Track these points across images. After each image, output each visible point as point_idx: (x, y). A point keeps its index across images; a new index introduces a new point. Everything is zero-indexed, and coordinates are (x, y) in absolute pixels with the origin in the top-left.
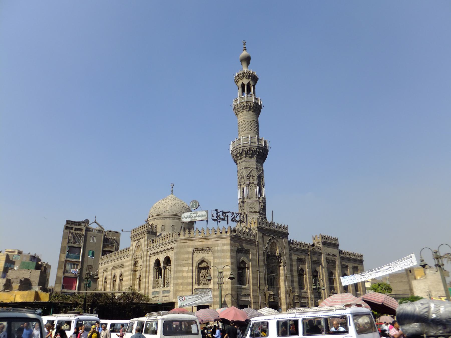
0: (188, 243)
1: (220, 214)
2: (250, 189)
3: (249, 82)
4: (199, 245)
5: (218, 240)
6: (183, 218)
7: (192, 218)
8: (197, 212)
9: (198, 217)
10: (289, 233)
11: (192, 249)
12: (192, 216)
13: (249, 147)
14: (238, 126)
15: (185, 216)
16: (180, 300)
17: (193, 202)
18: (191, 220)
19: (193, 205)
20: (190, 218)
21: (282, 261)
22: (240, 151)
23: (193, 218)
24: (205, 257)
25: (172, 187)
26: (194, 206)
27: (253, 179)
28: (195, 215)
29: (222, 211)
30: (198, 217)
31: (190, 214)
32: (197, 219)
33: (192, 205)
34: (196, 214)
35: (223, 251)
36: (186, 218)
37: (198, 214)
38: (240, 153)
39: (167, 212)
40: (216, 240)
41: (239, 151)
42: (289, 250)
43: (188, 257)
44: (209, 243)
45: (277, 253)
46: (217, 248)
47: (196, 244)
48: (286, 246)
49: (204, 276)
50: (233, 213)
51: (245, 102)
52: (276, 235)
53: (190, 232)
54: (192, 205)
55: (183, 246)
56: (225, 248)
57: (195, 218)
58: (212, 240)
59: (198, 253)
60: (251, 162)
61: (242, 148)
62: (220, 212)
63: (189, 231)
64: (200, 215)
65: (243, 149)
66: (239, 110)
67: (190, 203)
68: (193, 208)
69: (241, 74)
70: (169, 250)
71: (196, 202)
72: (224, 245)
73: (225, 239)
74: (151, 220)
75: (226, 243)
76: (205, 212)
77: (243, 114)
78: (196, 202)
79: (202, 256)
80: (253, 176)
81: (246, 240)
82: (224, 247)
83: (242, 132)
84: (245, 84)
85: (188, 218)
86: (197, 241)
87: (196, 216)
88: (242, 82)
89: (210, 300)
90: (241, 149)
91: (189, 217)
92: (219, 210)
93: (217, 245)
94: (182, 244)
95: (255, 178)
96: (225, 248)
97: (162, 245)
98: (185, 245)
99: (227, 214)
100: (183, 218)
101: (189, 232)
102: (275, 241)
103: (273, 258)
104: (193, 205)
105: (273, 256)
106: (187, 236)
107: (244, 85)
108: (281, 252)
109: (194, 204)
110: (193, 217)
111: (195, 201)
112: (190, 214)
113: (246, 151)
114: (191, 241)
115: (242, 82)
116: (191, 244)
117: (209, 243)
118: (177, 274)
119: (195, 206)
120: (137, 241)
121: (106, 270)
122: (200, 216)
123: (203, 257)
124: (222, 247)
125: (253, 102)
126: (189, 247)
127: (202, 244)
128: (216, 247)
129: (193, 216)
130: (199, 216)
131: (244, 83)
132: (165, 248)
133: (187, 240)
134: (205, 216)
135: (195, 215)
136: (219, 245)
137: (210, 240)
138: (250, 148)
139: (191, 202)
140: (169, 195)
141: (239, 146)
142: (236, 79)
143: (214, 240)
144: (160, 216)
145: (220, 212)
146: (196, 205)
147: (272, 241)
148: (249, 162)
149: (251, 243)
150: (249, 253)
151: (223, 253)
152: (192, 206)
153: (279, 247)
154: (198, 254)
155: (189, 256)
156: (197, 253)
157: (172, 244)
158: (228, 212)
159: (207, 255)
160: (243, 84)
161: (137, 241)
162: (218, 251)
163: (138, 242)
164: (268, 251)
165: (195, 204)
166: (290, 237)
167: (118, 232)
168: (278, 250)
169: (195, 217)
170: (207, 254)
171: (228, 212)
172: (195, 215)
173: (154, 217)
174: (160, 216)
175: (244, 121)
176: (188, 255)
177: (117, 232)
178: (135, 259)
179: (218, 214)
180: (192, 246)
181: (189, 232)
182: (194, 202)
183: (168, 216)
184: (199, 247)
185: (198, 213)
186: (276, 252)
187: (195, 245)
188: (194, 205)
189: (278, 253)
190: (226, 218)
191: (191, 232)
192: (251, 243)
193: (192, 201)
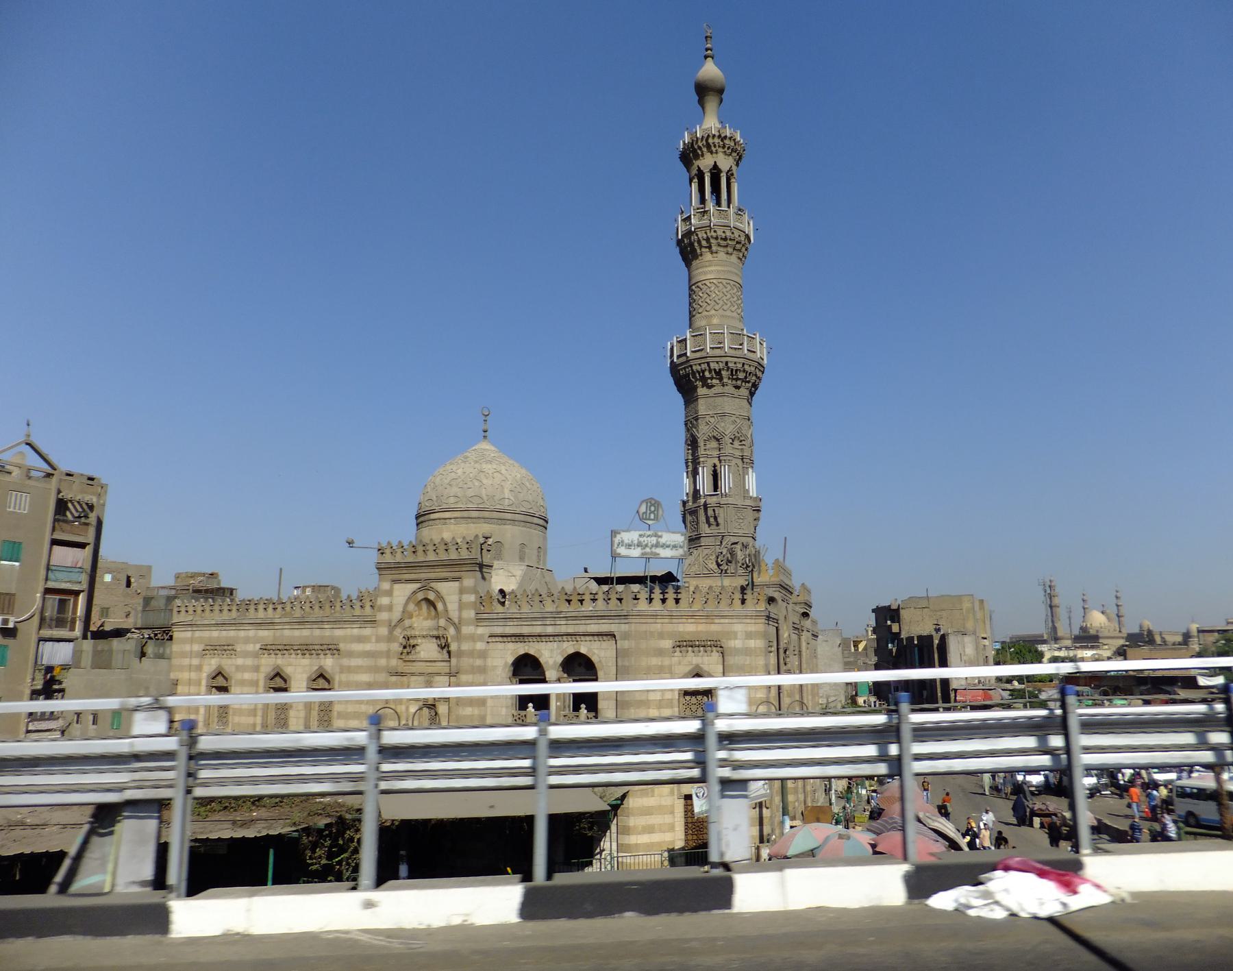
0: (659, 625)
4: (688, 633)
5: (735, 621)
6: (618, 545)
7: (644, 549)
8: (660, 534)
9: (661, 549)
11: (671, 641)
12: (646, 542)
14: (742, 297)
15: (626, 541)
16: (697, 796)
17: (649, 504)
18: (642, 554)
19: (648, 512)
20: (639, 548)
23: (648, 550)
24: (701, 666)
25: (484, 418)
26: (650, 516)
28: (654, 540)
30: (662, 546)
31: (640, 536)
32: (659, 554)
33: (645, 511)
34: (657, 540)
35: (747, 652)
36: (629, 546)
37: (662, 541)
39: (507, 502)
40: (730, 621)
43: (660, 664)
44: (714, 628)
46: (733, 642)
47: (681, 628)
51: (730, 227)
53: (664, 596)
54: (646, 513)
55: (646, 632)
56: (752, 643)
57: (654, 550)
58: (722, 621)
59: (684, 654)
60: (738, 400)
61: (724, 359)
63: (661, 591)
64: (668, 543)
65: (727, 363)
67: (640, 507)
68: (646, 519)
69: (714, 136)
70: (588, 638)
71: (656, 505)
72: (749, 636)
73: (753, 621)
74: (452, 521)
75: (755, 632)
76: (682, 535)
77: (716, 259)
78: (656, 505)
79: (694, 662)
80: (741, 439)
82: (751, 641)
84: (723, 170)
85: (633, 547)
86: (684, 620)
87: (657, 545)
88: (715, 162)
89: (764, 792)
90: (722, 362)
91: (638, 546)
93: (734, 635)
94: (644, 628)
95: (744, 445)
96: (752, 643)
97: (555, 618)
98: (652, 630)
100: (618, 545)
101: (661, 593)
104: (648, 512)
106: (657, 604)
107: (720, 171)
109: (650, 510)
110: (646, 545)
111: (653, 502)
112: (640, 536)
114: (666, 621)
115: (715, 162)
116: (669, 628)
117: (714, 628)
118: (633, 711)
119: (654, 514)
120: (418, 585)
122: (668, 546)
123: (697, 666)
124: (747, 641)
125: (744, 232)
126: (661, 636)
127: (695, 630)
128: (731, 639)
129: (647, 543)
130: (664, 546)
132: (563, 629)
133: (659, 617)
134: (681, 547)
135: (655, 542)
136: (739, 634)
137: (717, 621)
138: (743, 364)
139: (643, 502)
140: (473, 446)
141: (717, 352)
143: (727, 621)
144: (486, 514)
146: (656, 512)
148: (734, 399)
151: (748, 658)
152: (643, 513)
154: (684, 655)
155: (662, 661)
156: (679, 654)
157: (604, 621)
159: (706, 659)
160: (715, 166)
161: (418, 585)
162: (737, 651)
165: (653, 509)
167: (94, 477)
169: (652, 546)
170: (707, 658)
172: (654, 540)
173: (465, 514)
174: (486, 514)
175: (720, 281)
176: (660, 659)
177: (91, 479)
180: (670, 635)
181: (661, 593)
182: (650, 502)
183: (509, 516)
184: (688, 638)
185: (661, 537)
187: (679, 632)
188: (653, 512)
191: (666, 596)
193: (646, 501)
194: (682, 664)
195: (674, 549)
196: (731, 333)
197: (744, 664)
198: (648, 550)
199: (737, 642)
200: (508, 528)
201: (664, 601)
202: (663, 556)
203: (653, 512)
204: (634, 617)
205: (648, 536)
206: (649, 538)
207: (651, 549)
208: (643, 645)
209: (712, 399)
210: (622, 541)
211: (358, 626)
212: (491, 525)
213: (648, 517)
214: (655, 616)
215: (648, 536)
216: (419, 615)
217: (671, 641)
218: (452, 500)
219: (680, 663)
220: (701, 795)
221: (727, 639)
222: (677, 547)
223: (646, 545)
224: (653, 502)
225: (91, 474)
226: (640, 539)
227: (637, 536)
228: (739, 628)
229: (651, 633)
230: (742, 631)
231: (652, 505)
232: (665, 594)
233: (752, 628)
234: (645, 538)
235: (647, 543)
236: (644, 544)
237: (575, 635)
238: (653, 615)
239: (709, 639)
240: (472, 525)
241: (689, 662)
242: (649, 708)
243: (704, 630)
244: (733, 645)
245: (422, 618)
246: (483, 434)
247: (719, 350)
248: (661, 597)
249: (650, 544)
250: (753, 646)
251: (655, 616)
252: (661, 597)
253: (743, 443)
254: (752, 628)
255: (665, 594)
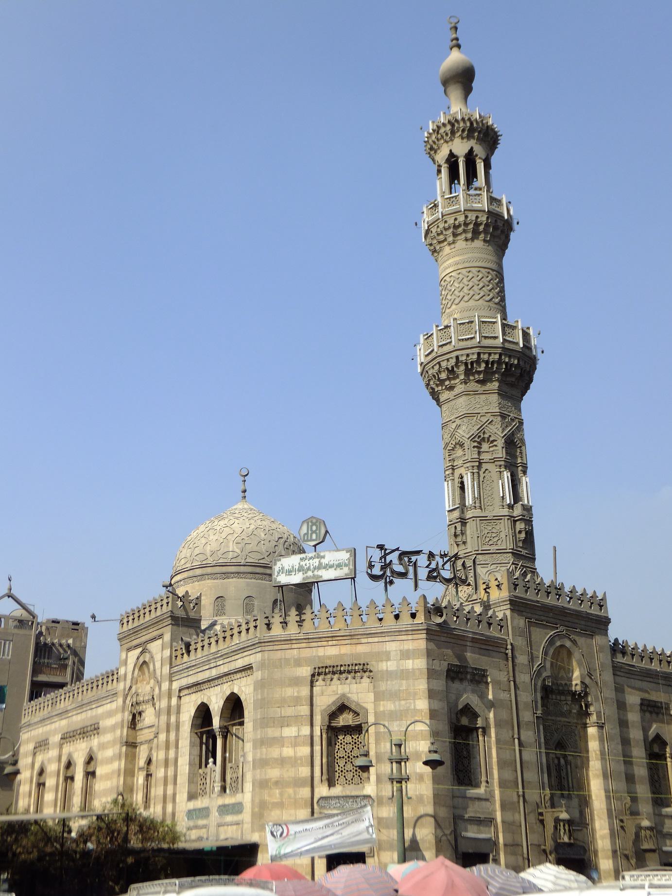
0: (295, 651)
1: (394, 557)
2: (481, 479)
3: (472, 148)
4: (329, 657)
5: (387, 639)
6: (278, 573)
7: (306, 573)
8: (322, 554)
10: (610, 619)
11: (309, 668)
12: (308, 565)
13: (476, 350)
15: (286, 568)
17: (310, 524)
19: (310, 532)
20: (301, 573)
21: (592, 709)
22: (449, 363)
23: (310, 573)
24: (349, 695)
25: (243, 479)
27: (491, 449)
28: (316, 562)
29: (397, 549)
30: (325, 568)
31: (301, 559)
32: (321, 576)
34: (319, 561)
36: (289, 572)
37: (324, 561)
38: (447, 369)
39: (231, 555)
40: (381, 639)
41: (444, 364)
42: (614, 674)
43: (296, 694)
44: (361, 649)
45: (574, 683)
46: (384, 663)
47: (321, 652)
48: (605, 658)
49: (349, 757)
50: (431, 555)
52: (566, 623)
55: (281, 659)
56: (409, 664)
57: (316, 573)
58: (370, 640)
59: (328, 682)
61: (454, 354)
62: (393, 551)
63: (297, 613)
64: (331, 563)
65: (457, 357)
66: (441, 237)
69: (444, 125)
70: (239, 675)
71: (318, 524)
72: (406, 655)
73: (410, 637)
76: (347, 552)
77: (453, 250)
79: (339, 692)
81: (474, 640)
83: (454, 307)
85: (294, 573)
86: (325, 643)
87: (319, 567)
88: (451, 151)
91: (299, 571)
92: (389, 546)
93: (387, 656)
96: (409, 664)
99: (414, 558)
100: (278, 573)
102: (568, 644)
103: (563, 698)
104: (310, 532)
105: (562, 693)
106: (293, 629)
107: (457, 157)
108: (587, 681)
110: (309, 569)
111: (314, 521)
112: (301, 559)
113: (466, 364)
114: (304, 645)
115: (451, 151)
116: (307, 653)
117: (361, 649)
119: (316, 534)
120: (140, 650)
121: (42, 745)
122: (331, 567)
123: (343, 695)
126: (298, 663)
130: (328, 567)
131: (455, 152)
132: (224, 669)
133: (294, 642)
134: (346, 565)
136: (392, 654)
139: (303, 522)
142: (430, 141)
143: (376, 639)
145: (393, 551)
146: (318, 532)
147: (558, 644)
148: (477, 396)
149: (490, 648)
150: (487, 680)
151: (404, 682)
153: (580, 664)
154: (328, 684)
155: (298, 692)
157: (245, 654)
158: (418, 553)
159: (354, 687)
160: (452, 155)
161: (140, 650)
162: (389, 675)
163: (142, 653)
164: (545, 674)
165: (314, 528)
166: (615, 632)
167: (79, 622)
168: (576, 674)
169: (315, 568)
171: (418, 553)
172: (316, 562)
176: (296, 689)
178: (132, 705)
179: (385, 560)
180: (308, 661)
182: (312, 522)
184: (329, 663)
185: (323, 557)
186: (570, 680)
188: (315, 532)
189: (578, 682)
190: (411, 569)
191: (303, 617)
192: (490, 648)
194: (325, 694)
195: (338, 569)
196: (460, 324)
197: (399, 690)
198: (310, 573)
199: (389, 663)
200: (233, 581)
201: (285, 623)
202: (326, 579)
203: (315, 532)
204: (266, 644)
205: (310, 558)
206: (311, 561)
207: (313, 572)
208: (277, 674)
209: (454, 402)
210: (283, 568)
211: (109, 701)
212: (215, 581)
213: (309, 538)
214: (289, 641)
215: (310, 558)
216: (143, 680)
217: (309, 668)
218: (183, 562)
219: (322, 694)
220: (279, 833)
221: (377, 661)
222: (342, 566)
223: (309, 569)
224: (314, 521)
225: (75, 620)
226: (301, 563)
227: (299, 560)
228: (392, 647)
229: (287, 660)
230: (396, 650)
231: (313, 524)
232: (302, 616)
233: (410, 646)
234: (307, 561)
235: (310, 567)
236: (305, 567)
237: (230, 674)
238: (287, 640)
239: (355, 662)
240: (196, 583)
241: (334, 691)
242: (283, 746)
243: (349, 652)
244: (385, 668)
245: (145, 683)
246: (242, 494)
247: (448, 346)
248: (298, 619)
249: (312, 567)
250: (411, 667)
251: (289, 641)
252: (298, 619)
253: (495, 443)
254: (410, 646)
255: (302, 616)
